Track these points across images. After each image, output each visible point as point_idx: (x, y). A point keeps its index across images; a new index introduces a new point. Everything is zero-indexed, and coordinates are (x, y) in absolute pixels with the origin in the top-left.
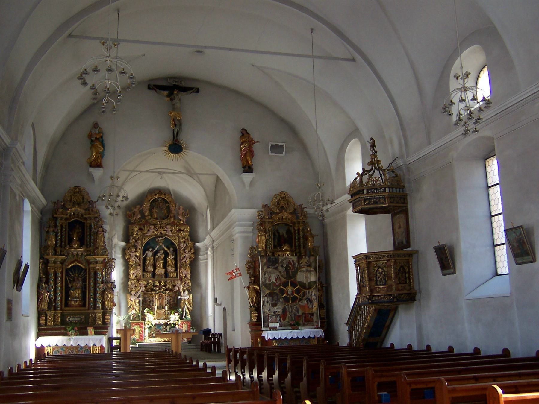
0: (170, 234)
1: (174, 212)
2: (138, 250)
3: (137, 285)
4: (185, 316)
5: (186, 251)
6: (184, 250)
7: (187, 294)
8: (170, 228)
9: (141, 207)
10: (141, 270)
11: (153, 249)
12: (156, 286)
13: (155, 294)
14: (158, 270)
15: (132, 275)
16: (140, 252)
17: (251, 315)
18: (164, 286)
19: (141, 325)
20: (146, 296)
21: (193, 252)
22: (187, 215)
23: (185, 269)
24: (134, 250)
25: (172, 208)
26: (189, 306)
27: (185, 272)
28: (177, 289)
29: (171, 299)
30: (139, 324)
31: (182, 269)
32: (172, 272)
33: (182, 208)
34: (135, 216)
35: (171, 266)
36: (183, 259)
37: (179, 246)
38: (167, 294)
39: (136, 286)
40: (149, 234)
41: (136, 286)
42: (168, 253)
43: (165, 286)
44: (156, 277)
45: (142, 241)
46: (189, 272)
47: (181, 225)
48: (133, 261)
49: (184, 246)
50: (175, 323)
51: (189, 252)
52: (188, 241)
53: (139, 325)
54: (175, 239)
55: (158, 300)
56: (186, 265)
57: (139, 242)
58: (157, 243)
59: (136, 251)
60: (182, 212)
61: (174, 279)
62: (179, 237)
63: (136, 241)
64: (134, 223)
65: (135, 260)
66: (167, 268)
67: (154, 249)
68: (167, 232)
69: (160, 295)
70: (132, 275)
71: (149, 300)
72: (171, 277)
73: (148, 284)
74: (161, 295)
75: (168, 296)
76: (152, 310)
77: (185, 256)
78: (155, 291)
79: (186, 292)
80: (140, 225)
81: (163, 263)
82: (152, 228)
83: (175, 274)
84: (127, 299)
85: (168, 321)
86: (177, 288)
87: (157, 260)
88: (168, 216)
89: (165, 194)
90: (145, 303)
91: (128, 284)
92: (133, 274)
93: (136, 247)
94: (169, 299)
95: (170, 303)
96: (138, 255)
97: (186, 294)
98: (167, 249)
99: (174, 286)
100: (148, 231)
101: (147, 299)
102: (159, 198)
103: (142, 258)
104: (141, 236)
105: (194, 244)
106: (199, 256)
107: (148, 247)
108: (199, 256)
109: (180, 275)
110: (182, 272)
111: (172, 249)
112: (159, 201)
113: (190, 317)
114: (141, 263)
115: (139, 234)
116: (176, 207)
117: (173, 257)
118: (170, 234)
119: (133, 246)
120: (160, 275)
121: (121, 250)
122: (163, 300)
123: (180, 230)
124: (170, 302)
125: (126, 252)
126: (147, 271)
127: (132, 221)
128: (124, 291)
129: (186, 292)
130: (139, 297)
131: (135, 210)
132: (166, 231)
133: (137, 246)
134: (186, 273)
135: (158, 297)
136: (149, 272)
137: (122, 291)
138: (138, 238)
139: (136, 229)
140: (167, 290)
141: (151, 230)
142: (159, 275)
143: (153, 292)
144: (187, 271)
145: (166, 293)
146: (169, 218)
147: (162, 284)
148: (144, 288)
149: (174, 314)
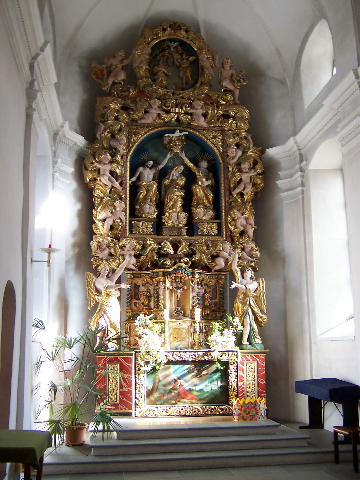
0: (202, 122)
1: (209, 72)
2: (119, 158)
3: (115, 250)
4: (249, 340)
5: (243, 166)
6: (238, 164)
7: (251, 278)
8: (202, 107)
9: (127, 57)
10: (125, 211)
11: (156, 163)
12: (166, 255)
13: (165, 274)
14: (170, 214)
15: (100, 224)
16: (124, 166)
17: (230, 351)
18: (186, 256)
19: (126, 364)
20: (139, 282)
21: (260, 171)
22: (242, 80)
23: (243, 214)
24: (110, 157)
25: (205, 61)
26: (257, 310)
27: (241, 221)
28: (223, 264)
29: (206, 292)
30: (119, 358)
31: (236, 214)
32: (206, 221)
33: (229, 63)
34: (112, 74)
35: (203, 204)
36: (235, 188)
37: (224, 155)
38: (197, 276)
39: (111, 255)
40: (149, 119)
41: (111, 255)
42: (194, 175)
43: (190, 255)
44: (165, 232)
45: (129, 138)
46: (252, 222)
47: (228, 105)
48: (106, 185)
49: (236, 154)
50: (225, 358)
51: (250, 169)
52: (248, 141)
53: (118, 361)
54: (214, 137)
55: (171, 291)
56: (244, 203)
57: (123, 137)
58: (167, 148)
59: (111, 162)
60: (230, 74)
61: (214, 238)
62: (223, 132)
63: (113, 136)
64: (109, 94)
65: (109, 184)
66: (194, 209)
67: (160, 164)
68: (195, 117)
69: (178, 280)
70: (100, 224)
71: (148, 292)
72: (203, 235)
73: (144, 247)
74: (181, 279)
75: (198, 284)
76: (156, 319)
77: (240, 181)
78: (163, 266)
79: (249, 273)
80: (124, 98)
81: (183, 198)
82: (155, 107)
83: (215, 226)
84: (87, 284)
85: (206, 353)
86: (221, 263)
87: (166, 191)
88: (196, 82)
89: (187, 31)
90: (134, 301)
91: (90, 247)
92: (104, 220)
93: (114, 151)
94: (201, 291)
95: (204, 303)
96: (118, 171)
97: (248, 279)
98: (191, 165)
99: (214, 257)
100: (146, 112)
101: (142, 288)
102: (170, 40)
103: (129, 183)
104: (127, 124)
105: (263, 152)
106: (277, 182)
107: (144, 157)
108: (277, 182)
109: (227, 226)
110: (233, 220)
111: (204, 164)
112: (172, 49)
113: (260, 342)
114: (126, 194)
115: (121, 118)
116: (213, 59)
117: (209, 183)
118: (202, 122)
119: (103, 148)
120: (176, 229)
121: (74, 157)
122: (185, 293)
123: (226, 116)
124: (203, 299)
125: (87, 163)
126: (141, 217)
127: (105, 89)
128: (78, 267)
129: (249, 273)
130: (119, 281)
131: (113, 62)
132: (191, 114)
133: (116, 149)
134: (244, 222)
135: (172, 285)
136: (148, 220)
137: (72, 266)
138: (120, 130)
139: (115, 106)
140: (194, 266)
141: (152, 111)
142: (173, 227)
143: (158, 270)
144: (246, 219)
145: (193, 274)
146: (198, 85)
147: (184, 248)
148: (134, 260)
149: (222, 334)
